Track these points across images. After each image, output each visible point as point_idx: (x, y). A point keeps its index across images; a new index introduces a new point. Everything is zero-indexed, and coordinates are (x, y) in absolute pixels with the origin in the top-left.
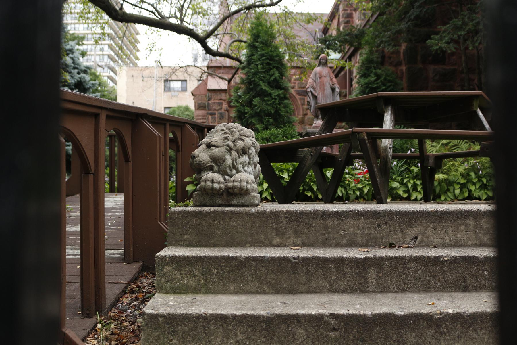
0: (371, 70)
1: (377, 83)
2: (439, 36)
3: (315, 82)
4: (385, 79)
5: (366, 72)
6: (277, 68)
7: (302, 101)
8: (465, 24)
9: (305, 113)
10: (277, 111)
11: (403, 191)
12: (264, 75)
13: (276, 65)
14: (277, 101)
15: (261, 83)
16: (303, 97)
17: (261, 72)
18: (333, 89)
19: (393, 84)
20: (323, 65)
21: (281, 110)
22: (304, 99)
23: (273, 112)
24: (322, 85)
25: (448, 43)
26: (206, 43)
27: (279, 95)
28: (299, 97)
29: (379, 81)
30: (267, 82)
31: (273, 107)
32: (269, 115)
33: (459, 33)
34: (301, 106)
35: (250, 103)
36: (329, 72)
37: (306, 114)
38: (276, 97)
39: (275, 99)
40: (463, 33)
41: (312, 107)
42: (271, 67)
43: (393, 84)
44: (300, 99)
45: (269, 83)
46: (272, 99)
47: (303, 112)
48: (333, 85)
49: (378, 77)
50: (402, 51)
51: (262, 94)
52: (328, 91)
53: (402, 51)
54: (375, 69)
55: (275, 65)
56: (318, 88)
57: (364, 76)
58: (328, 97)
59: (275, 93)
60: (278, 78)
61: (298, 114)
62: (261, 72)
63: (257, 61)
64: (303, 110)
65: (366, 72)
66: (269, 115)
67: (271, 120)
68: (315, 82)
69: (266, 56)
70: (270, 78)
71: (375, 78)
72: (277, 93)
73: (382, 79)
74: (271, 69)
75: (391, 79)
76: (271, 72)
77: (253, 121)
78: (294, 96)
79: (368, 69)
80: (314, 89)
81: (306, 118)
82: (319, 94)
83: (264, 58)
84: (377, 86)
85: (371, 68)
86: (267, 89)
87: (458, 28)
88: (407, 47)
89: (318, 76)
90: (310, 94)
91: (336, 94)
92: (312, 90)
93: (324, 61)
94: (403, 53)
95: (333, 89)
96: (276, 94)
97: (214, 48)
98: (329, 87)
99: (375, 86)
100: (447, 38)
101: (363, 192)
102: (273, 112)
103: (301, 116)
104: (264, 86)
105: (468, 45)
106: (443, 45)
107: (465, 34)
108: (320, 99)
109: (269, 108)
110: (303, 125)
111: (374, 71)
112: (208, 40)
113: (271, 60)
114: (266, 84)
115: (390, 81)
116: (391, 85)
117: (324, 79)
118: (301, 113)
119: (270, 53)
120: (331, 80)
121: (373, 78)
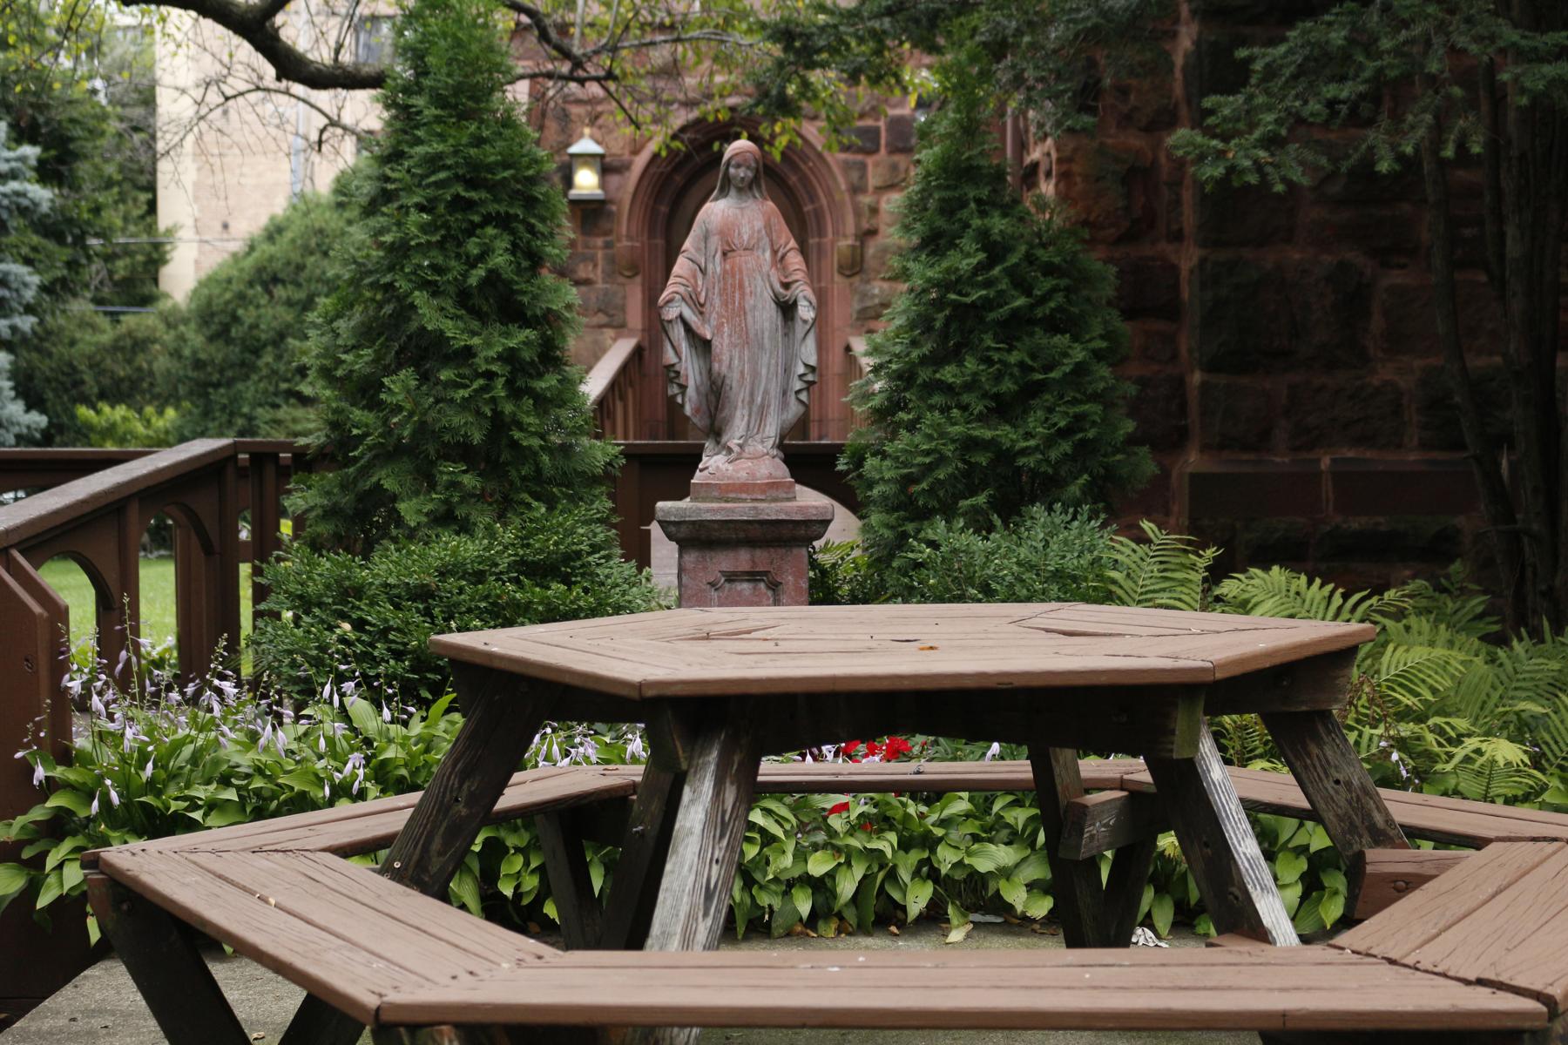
0: (964, 214)
1: (988, 284)
2: (1240, 98)
3: (704, 272)
4: (1030, 258)
5: (940, 222)
6: (504, 222)
7: (855, 175)
8: (1364, 42)
9: (865, 226)
10: (499, 426)
11: (1030, 887)
12: (440, 260)
13: (502, 209)
14: (500, 383)
15: (419, 298)
16: (859, 157)
17: (423, 248)
18: (787, 309)
19: (1064, 282)
20: (740, 190)
21: (521, 427)
22: (863, 167)
23: (477, 437)
24: (733, 286)
25: (1272, 142)
26: (274, 36)
27: (509, 357)
28: (843, 156)
29: (996, 271)
30: (452, 289)
31: (478, 413)
32: (464, 452)
33: (1330, 91)
34: (847, 197)
35: (366, 391)
36: (768, 226)
37: (873, 232)
38: (494, 368)
39: (490, 375)
40: (1346, 91)
41: (691, 391)
42: (476, 219)
43: (1064, 282)
44: (847, 167)
45: (464, 298)
46: (478, 375)
47: (857, 225)
48: (786, 286)
49: (994, 250)
50: (1179, 60)
51: (425, 352)
52: (765, 316)
53: (1179, 60)
54: (983, 214)
55: (493, 208)
56: (717, 302)
57: (935, 243)
58: (761, 347)
59: (493, 343)
60: (508, 273)
61: (836, 232)
62: (423, 248)
63: (408, 189)
64: (858, 214)
65: (940, 222)
66: (464, 452)
67: (468, 480)
68: (704, 272)
69: (449, 168)
70: (465, 275)
71: (981, 256)
72: (500, 344)
73: (1013, 259)
74: (471, 231)
75: (1057, 260)
76: (472, 246)
77: (388, 484)
78: (820, 156)
79: (949, 209)
80: (699, 308)
81: (871, 249)
82: (718, 329)
83: (442, 175)
84: (985, 299)
85: (963, 204)
86: (450, 328)
87: (1321, 65)
88: (1197, 43)
89: (715, 242)
90: (678, 332)
91: (800, 329)
92: (688, 314)
93: (742, 173)
94: (1184, 69)
95: (787, 309)
96: (492, 353)
97: (321, 55)
98: (768, 295)
99: (976, 295)
100: (1270, 117)
101: (834, 895)
102: (477, 437)
103: (846, 243)
104: (430, 314)
105: (1371, 148)
106: (1243, 154)
107: (1362, 97)
108: (726, 358)
109: (458, 420)
110: (856, 280)
111: (976, 222)
112: (279, 19)
113: (471, 184)
114: (448, 304)
115: (1050, 270)
116: (1054, 290)
117: (746, 261)
118: (850, 227)
119: (473, 151)
120: (779, 260)
121: (965, 259)
